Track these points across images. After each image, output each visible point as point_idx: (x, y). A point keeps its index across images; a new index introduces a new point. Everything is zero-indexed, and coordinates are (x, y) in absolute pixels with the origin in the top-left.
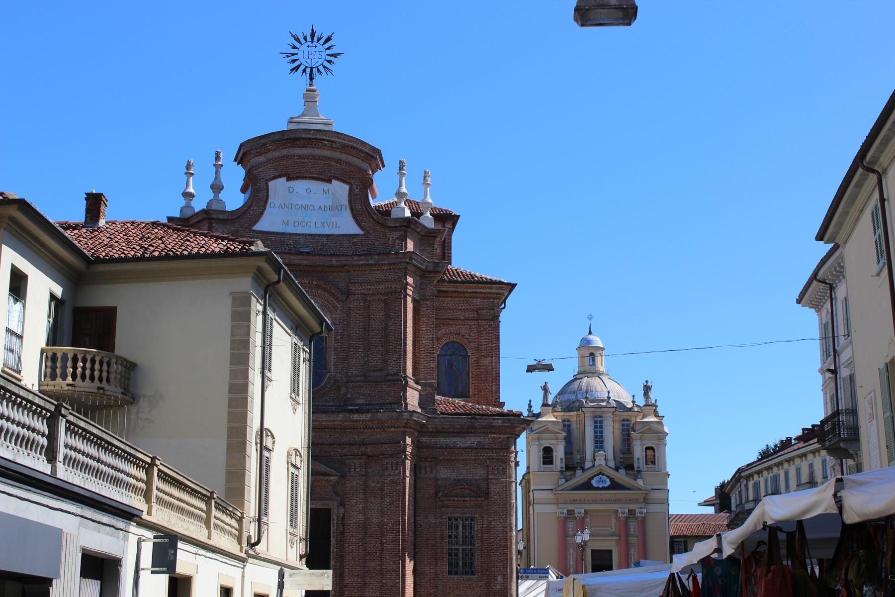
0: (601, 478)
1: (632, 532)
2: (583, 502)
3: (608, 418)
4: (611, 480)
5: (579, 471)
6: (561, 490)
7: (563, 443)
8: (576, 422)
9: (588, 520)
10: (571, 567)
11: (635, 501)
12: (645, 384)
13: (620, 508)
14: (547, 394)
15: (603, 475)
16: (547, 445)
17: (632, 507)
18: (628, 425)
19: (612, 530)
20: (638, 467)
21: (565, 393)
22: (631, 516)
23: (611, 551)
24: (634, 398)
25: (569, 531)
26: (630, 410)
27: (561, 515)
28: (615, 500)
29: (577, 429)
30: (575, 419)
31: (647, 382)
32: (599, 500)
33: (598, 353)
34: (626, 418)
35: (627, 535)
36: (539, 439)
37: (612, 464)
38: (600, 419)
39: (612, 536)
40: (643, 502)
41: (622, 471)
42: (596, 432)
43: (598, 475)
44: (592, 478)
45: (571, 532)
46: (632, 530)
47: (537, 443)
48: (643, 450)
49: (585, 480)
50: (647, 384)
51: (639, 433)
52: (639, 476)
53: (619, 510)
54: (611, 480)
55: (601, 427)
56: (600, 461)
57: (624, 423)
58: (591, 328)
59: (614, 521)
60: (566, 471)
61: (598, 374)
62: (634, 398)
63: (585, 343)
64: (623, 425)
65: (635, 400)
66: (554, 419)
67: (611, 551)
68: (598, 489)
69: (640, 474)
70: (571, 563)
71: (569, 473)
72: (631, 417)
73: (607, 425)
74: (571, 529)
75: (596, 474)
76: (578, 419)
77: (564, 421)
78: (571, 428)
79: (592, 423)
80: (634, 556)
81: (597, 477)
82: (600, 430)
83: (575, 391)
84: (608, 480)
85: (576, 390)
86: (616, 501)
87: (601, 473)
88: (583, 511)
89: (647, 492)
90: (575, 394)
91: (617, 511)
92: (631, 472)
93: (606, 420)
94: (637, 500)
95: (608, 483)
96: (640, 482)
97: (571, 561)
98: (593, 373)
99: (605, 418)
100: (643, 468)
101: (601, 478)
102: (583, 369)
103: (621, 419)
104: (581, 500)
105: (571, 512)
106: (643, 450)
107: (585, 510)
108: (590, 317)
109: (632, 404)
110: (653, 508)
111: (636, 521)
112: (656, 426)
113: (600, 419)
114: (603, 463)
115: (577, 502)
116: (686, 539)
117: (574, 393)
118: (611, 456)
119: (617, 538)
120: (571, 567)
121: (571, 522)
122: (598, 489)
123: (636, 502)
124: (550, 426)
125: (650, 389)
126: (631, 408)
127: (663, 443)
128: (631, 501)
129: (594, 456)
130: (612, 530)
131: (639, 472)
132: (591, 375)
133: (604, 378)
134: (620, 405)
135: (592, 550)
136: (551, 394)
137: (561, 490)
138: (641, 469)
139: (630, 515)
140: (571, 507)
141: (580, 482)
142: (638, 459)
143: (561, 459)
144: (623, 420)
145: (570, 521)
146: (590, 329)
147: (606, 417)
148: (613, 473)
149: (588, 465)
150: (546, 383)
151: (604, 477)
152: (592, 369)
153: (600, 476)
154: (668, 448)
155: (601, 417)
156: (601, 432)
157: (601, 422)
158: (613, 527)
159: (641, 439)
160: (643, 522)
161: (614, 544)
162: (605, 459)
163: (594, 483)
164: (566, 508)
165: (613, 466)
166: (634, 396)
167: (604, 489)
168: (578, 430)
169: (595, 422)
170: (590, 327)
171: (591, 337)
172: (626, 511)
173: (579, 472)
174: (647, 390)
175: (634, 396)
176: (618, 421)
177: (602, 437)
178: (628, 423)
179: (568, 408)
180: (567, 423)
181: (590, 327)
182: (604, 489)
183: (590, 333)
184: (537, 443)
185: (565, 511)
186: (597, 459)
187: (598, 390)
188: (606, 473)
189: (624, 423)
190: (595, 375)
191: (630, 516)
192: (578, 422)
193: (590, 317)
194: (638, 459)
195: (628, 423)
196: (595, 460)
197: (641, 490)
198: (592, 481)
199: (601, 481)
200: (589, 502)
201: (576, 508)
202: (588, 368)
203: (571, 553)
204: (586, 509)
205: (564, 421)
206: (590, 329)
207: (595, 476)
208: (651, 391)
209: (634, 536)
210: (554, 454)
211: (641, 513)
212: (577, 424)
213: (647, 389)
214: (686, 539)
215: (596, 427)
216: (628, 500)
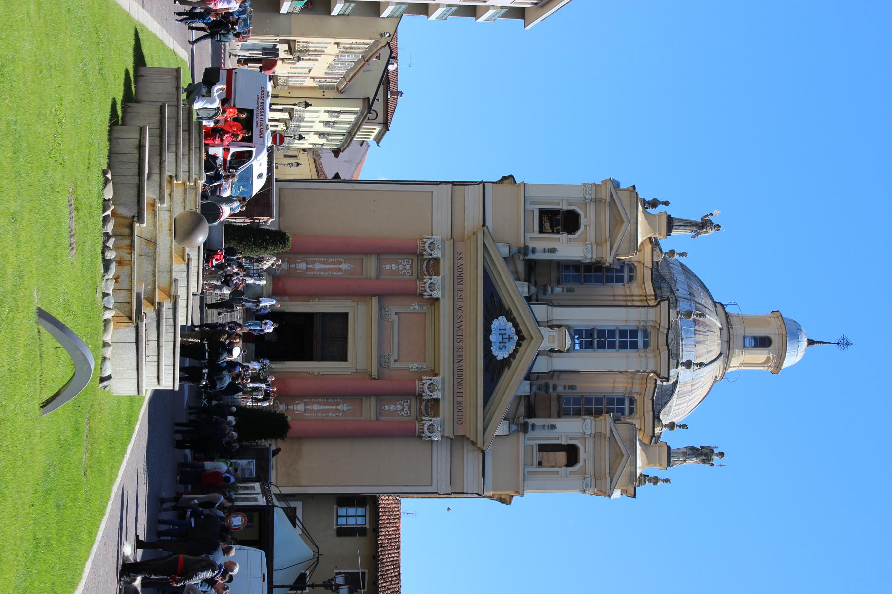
0: (510, 338)
1: (387, 408)
2: (457, 295)
3: (643, 360)
4: (507, 363)
5: (526, 289)
6: (484, 243)
7: (589, 256)
8: (628, 293)
9: (415, 307)
10: (311, 266)
11: (458, 418)
12: (716, 451)
13: (443, 380)
14: (695, 228)
15: (519, 344)
16: (583, 221)
17: (445, 408)
18: (622, 411)
19: (393, 361)
20: (533, 426)
21: (687, 277)
22: (423, 408)
23: (343, 357)
24: (680, 426)
25: (391, 264)
26: (656, 418)
27: (427, 245)
28: (461, 370)
29: (614, 295)
30: (636, 290)
31: (721, 454)
32: (460, 332)
33: (771, 356)
34: (638, 407)
35: (381, 396)
36: (597, 201)
37: (542, 366)
38: (641, 344)
39: (380, 364)
40: (455, 434)
41: (525, 388)
42: (612, 333)
43: (518, 332)
44: (511, 319)
45: (388, 267)
46: (393, 408)
47: (588, 197)
48: (571, 439)
49: (508, 303)
50: (717, 455)
51: (611, 431)
52: (514, 427)
53: (438, 378)
54: (507, 363)
55: (623, 346)
56: (549, 339)
57: (627, 403)
58: (822, 345)
59: (413, 366)
60: (525, 260)
61: (725, 355)
62: (680, 426)
63: (792, 330)
64: (621, 401)
65: (677, 429)
66: (640, 240)
67: (343, 357)
68: (487, 331)
69: (518, 431)
70: (318, 266)
71: (521, 267)
72: (640, 418)
73: (627, 357)
74: (394, 267)
75: (521, 327)
76: (635, 298)
77: (632, 268)
78: (615, 284)
79: (631, 325)
80: (334, 411)
81: (514, 330)
82: (617, 344)
83: (694, 296)
84: (506, 356)
85: (697, 300)
86: (458, 372)
87: (521, 338)
88: (437, 294)
89: (479, 444)
90: (688, 297)
91: (436, 375)
92: (522, 410)
93: (640, 356)
94: (461, 421)
95: (500, 355)
96: (502, 429)
97: (323, 266)
98: (729, 341)
99: (643, 354)
100: (529, 439)
101: (510, 338)
102: (735, 321)
103: (636, 397)
104: (461, 290)
105: (433, 266)
106: (571, 439)
107: (437, 300)
108: (844, 343)
109: (667, 422)
110: (441, 458)
111: (415, 276)
112: (627, 470)
113: (641, 344)
114: (545, 345)
115: (456, 281)
116: (369, 533)
117: (690, 294)
118: (560, 363)
119: (375, 373)
120: (311, 266)
121: (412, 268)
122: (487, 331)
123: (456, 417)
124: (626, 228)
125: (704, 461)
126: (659, 420)
127: (587, 485)
128: (458, 405)
129: (559, 326)
130: (393, 361)
131: (525, 428)
132: (726, 338)
133: (719, 363)
134: (664, 397)
135: (347, 314)
136: (694, 237)
137: (484, 243)
138: (531, 434)
139: (426, 405)
140: (445, 267)
141: (498, 287)
142: (553, 427)
143: (553, 251)
144: (632, 401)
145: (412, 266)
146: (819, 342)
147: (646, 357)
148: (520, 368)
149: (541, 311)
150: (718, 226)
151: (512, 347)
152: (737, 341)
153: (516, 338)
154: (574, 496)
155: (646, 345)
156: (612, 346)
157: (634, 346)
158: (398, 365)
159: (597, 436)
160: (412, 434)
161: (361, 365)
162: (552, 351)
163: (500, 322)
164: (443, 255)
165: (535, 369)
166: (684, 426)
167: (487, 344)
168: (612, 298)
169: (634, 333)
170: (823, 342)
171: (804, 344)
172: (437, 395)
173: (524, 288)
174: (701, 454)
175: (684, 426)
176: (632, 387)
177: (601, 346)
178: (627, 411)
179: (659, 277)
180: (626, 274)
181: (823, 342)
182: (487, 344)
183: (811, 342)
184: (588, 197)
185: (436, 254)
186: (555, 332)
187: (699, 346)
188: (521, 350)
189: (627, 403)
190: (725, 345)
191: (424, 404)
192: (629, 298)
193: (844, 343)
194: (553, 427)
195: (627, 411)
196: (551, 327)
197: (484, 430)
198: (504, 318)
199: (505, 338)
200: (456, 309)
201: (443, 279)
202: (738, 331)
203: (342, 266)
204: (441, 300)
205: (632, 268)
206: (819, 342)
207: (516, 325)
208: (702, 465)
209: (379, 412)
210: (564, 236)
211: (431, 429)
212: (626, 295)
213: (706, 455)
214: (369, 533)
215: (623, 333)
216: (460, 400)
